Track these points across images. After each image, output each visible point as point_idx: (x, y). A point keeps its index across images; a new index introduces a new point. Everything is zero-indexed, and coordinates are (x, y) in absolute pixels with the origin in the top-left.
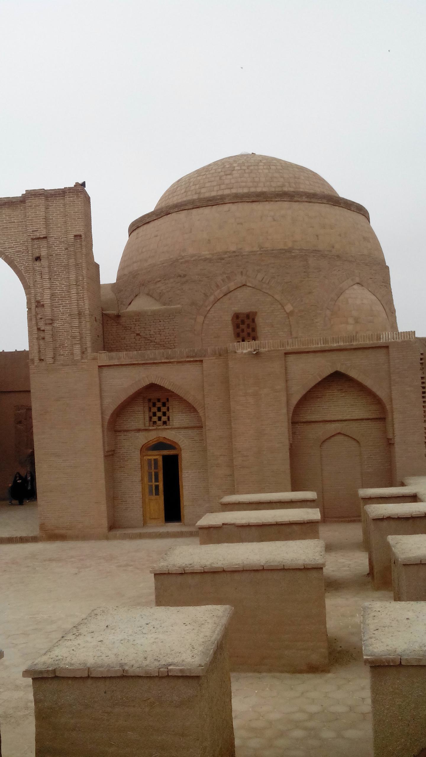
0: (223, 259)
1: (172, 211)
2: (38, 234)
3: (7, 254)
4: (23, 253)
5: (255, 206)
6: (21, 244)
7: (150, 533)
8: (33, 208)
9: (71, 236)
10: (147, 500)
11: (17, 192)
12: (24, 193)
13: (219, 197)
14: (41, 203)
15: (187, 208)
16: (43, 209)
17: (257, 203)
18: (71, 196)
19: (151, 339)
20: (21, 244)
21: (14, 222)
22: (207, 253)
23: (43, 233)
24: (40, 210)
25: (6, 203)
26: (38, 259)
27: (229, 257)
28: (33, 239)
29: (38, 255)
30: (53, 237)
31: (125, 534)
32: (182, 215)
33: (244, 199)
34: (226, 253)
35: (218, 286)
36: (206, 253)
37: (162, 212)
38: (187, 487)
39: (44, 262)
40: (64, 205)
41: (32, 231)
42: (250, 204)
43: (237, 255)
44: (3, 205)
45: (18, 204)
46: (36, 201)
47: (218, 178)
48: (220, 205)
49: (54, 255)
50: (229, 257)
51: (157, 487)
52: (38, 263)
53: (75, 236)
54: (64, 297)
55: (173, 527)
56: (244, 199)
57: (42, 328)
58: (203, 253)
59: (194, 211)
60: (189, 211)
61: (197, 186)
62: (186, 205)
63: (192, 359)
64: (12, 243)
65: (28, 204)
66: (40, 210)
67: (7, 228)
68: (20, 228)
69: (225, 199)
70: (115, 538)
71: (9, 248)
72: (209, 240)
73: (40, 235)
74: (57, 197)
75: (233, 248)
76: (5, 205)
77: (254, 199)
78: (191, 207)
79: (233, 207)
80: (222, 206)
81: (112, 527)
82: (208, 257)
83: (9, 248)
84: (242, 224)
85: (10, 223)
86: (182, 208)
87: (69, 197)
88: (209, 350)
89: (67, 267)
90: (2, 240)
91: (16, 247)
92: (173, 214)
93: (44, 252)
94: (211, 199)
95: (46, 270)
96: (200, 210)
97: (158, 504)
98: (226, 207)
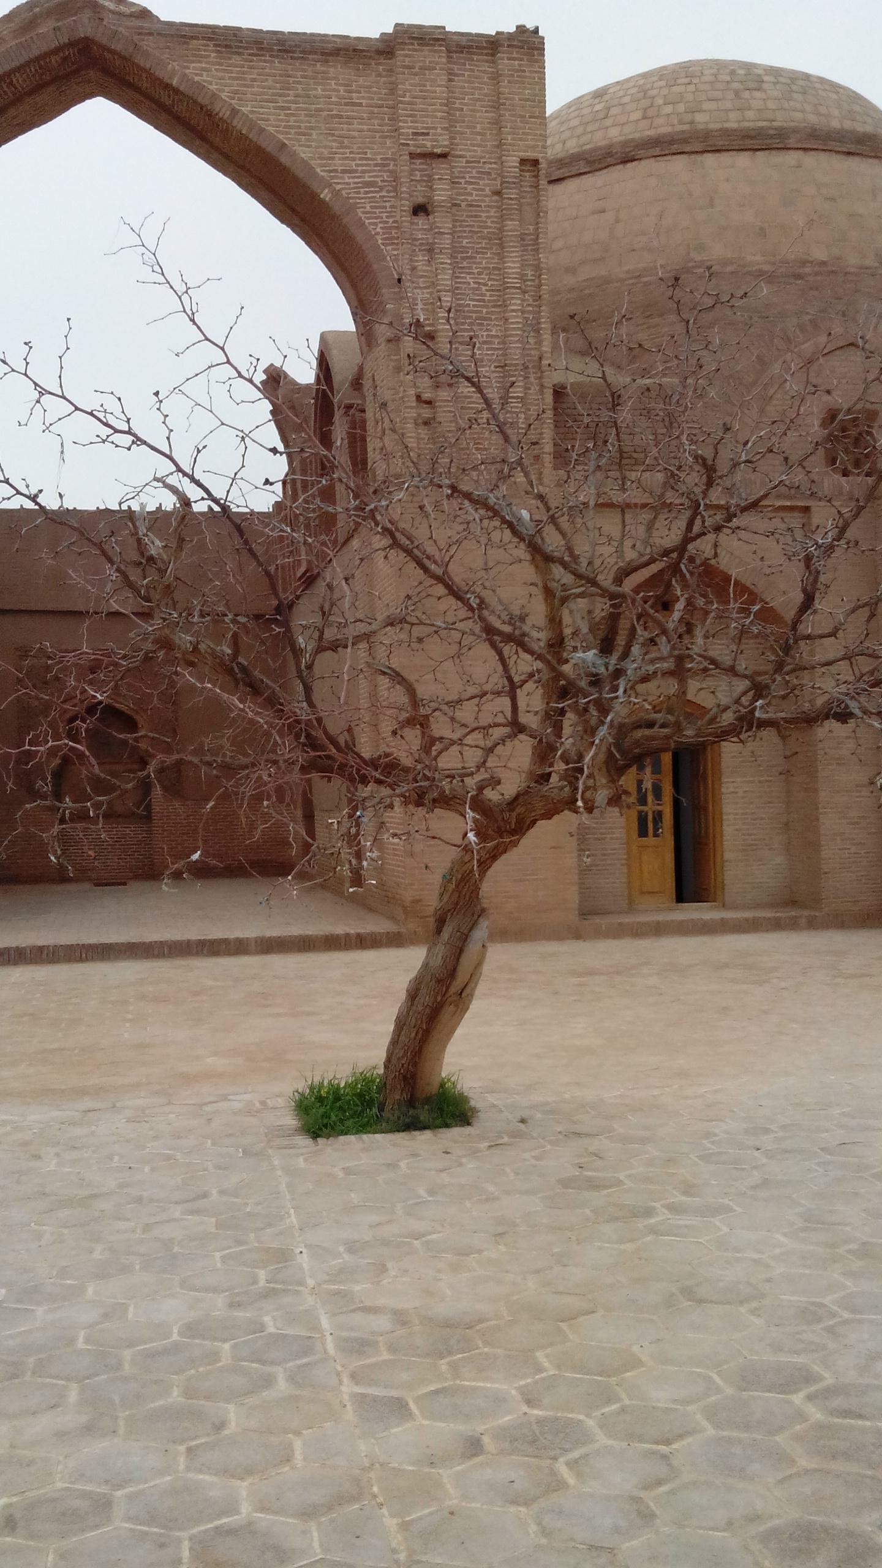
0: (799, 277)
1: (641, 153)
2: (428, 145)
3: (338, 187)
4: (381, 188)
5: (853, 162)
6: (376, 165)
7: (681, 923)
8: (416, 74)
9: (513, 161)
10: (634, 848)
11: (370, 24)
12: (390, 30)
13: (772, 132)
14: (437, 63)
15: (688, 149)
16: (442, 80)
17: (857, 159)
18: (515, 55)
19: (635, 455)
20: (376, 165)
21: (360, 105)
22: (759, 258)
23: (439, 142)
24: (435, 80)
25: (339, 49)
26: (420, 209)
27: (816, 274)
28: (412, 156)
29: (421, 200)
30: (461, 156)
31: (620, 924)
32: (678, 165)
33: (832, 145)
34: (804, 263)
35: (788, 340)
36: (755, 258)
37: (610, 154)
38: (731, 817)
39: (442, 221)
40: (496, 77)
41: (415, 134)
42: (842, 157)
43: (828, 270)
44: (331, 54)
45: (370, 57)
46: (425, 56)
47: (730, 95)
48: (774, 152)
49: (463, 204)
50: (816, 274)
51: (658, 816)
52: (421, 221)
53: (523, 161)
54: (485, 319)
55: (692, 912)
56: (832, 145)
57: (427, 396)
58: (750, 258)
59: (710, 159)
60: (693, 157)
61: (681, 108)
62: (686, 141)
63: (788, 504)
64: (354, 159)
65: (402, 57)
66: (435, 80)
67: (341, 117)
68: (376, 122)
69: (789, 138)
70: (598, 934)
71: (344, 172)
72: (762, 229)
73: (433, 147)
74: (475, 54)
75: (820, 254)
76: (338, 55)
77: (853, 148)
78: (698, 147)
79: (810, 160)
80: (782, 153)
81: (586, 912)
82: (765, 268)
83: (344, 172)
84: (833, 199)
85: (346, 104)
86: (675, 148)
87: (509, 59)
88: (826, 484)
89: (499, 241)
90: (325, 147)
91: (363, 172)
92: (643, 162)
93: (441, 194)
94: (752, 133)
95: (447, 240)
96: (725, 158)
97: (659, 856)
98: (792, 157)
